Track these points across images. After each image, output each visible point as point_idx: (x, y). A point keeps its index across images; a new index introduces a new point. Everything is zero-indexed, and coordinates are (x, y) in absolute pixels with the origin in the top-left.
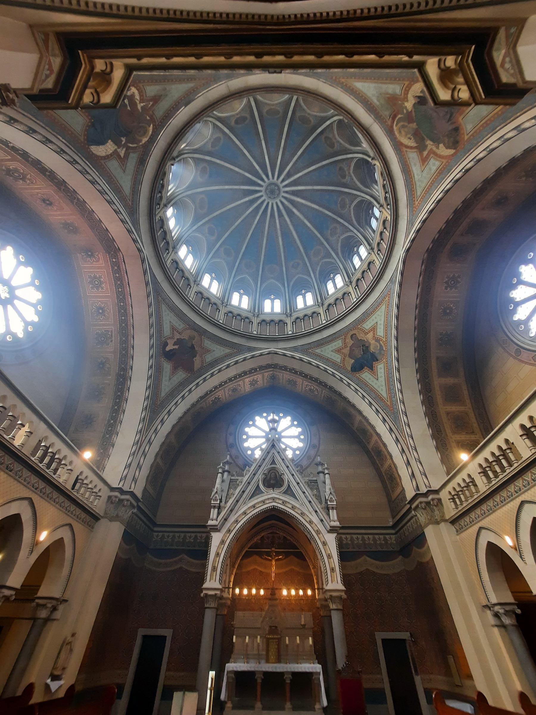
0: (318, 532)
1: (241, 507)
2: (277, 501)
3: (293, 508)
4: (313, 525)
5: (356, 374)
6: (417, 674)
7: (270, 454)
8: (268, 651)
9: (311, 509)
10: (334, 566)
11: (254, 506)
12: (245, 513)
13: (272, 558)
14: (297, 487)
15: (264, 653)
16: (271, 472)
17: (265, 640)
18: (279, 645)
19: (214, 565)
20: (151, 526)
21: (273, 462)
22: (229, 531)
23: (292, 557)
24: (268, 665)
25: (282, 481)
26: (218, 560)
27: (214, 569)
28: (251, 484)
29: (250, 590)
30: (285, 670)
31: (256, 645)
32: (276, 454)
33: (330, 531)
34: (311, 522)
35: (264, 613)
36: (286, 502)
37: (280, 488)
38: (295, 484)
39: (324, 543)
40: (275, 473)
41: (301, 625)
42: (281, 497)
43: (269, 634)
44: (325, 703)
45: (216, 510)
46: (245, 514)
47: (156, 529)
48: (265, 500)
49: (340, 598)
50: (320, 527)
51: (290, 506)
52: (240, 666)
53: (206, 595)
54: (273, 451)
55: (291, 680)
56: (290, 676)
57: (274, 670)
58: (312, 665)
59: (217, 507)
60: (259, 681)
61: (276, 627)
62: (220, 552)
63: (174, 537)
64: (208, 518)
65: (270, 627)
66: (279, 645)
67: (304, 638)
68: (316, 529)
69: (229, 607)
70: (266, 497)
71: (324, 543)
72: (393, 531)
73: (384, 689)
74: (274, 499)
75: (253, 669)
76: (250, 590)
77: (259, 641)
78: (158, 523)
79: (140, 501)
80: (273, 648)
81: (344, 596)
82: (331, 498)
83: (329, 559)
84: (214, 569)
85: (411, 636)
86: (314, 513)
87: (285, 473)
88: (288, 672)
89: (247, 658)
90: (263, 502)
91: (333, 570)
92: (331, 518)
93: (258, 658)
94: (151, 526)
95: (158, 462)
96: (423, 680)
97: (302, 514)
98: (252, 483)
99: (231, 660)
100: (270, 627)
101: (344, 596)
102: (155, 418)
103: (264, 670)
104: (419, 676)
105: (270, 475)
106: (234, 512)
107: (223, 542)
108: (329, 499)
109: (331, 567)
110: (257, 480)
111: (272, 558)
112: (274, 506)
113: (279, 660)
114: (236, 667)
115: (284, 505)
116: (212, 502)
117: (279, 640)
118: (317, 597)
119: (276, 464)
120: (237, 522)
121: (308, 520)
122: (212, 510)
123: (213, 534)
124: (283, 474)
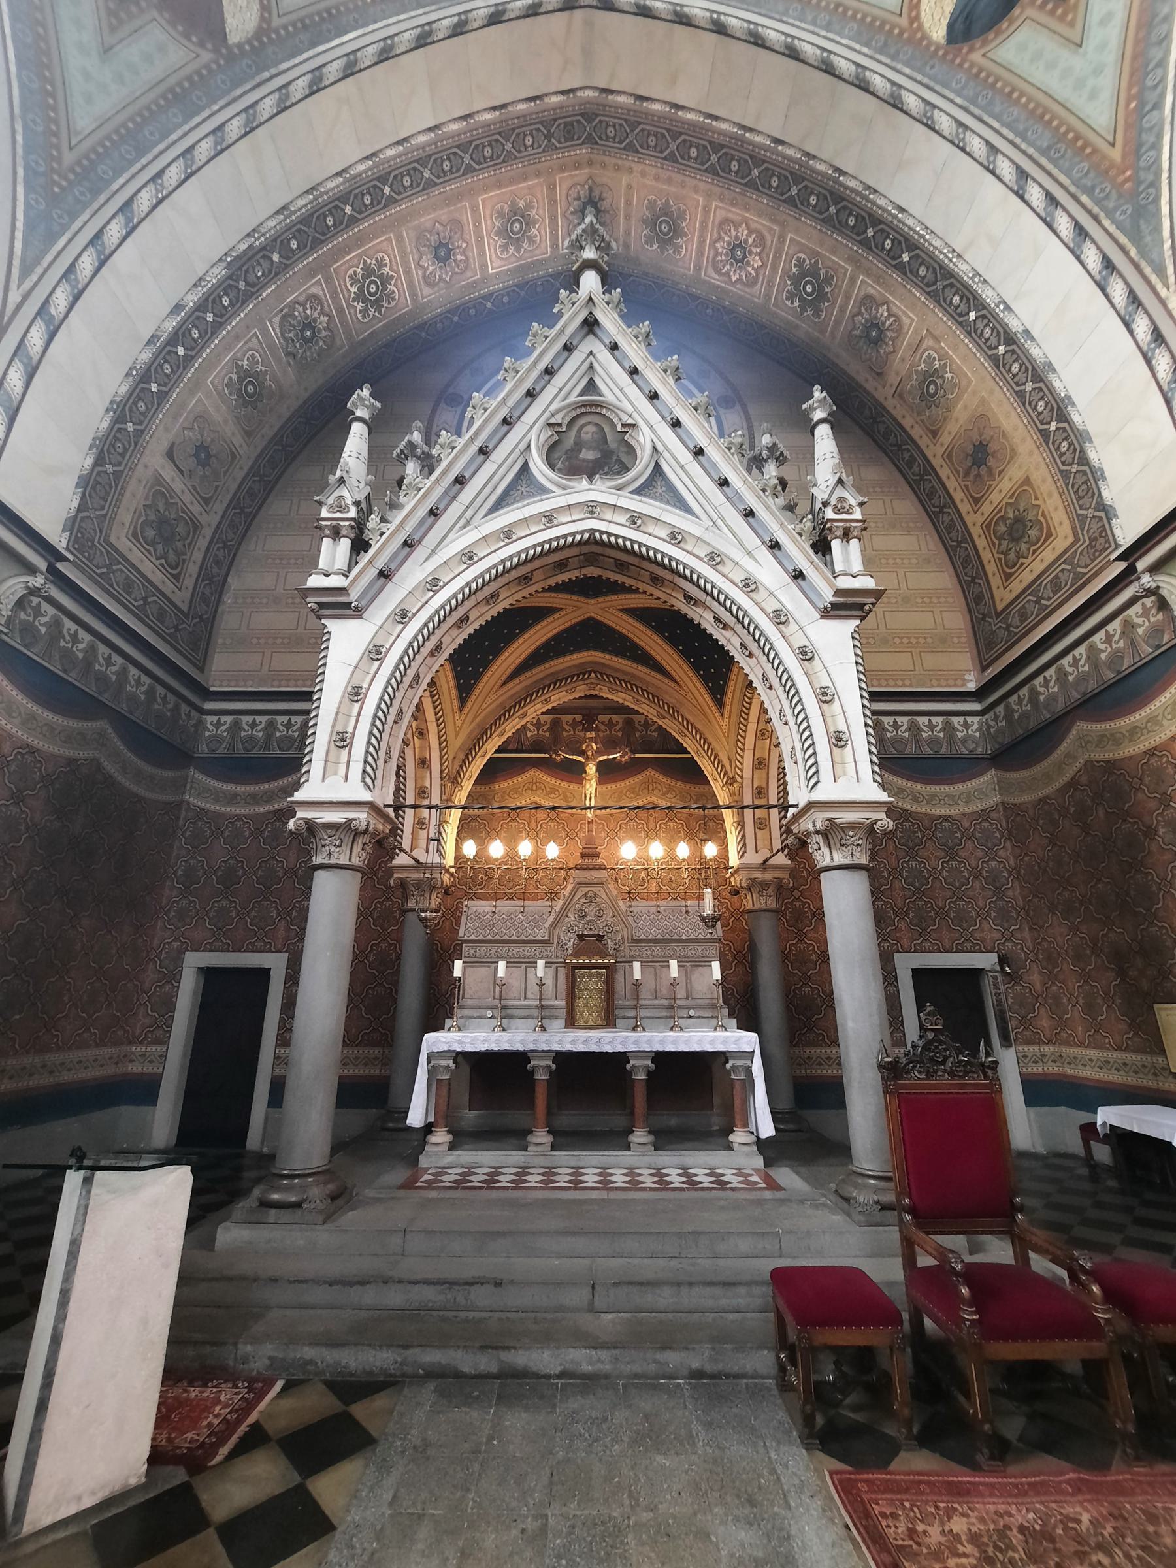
0: (780, 618)
1: (451, 536)
2: (608, 515)
3: (675, 537)
4: (761, 596)
5: (971, 50)
6: (1006, 1041)
7: (577, 357)
8: (571, 997)
9: (752, 541)
10: (842, 727)
11: (508, 534)
12: (468, 556)
13: (587, 758)
14: (694, 467)
15: (561, 1003)
16: (581, 422)
17: (562, 971)
18: (609, 984)
19: (339, 728)
20: (197, 701)
21: (591, 386)
22: (403, 616)
23: (650, 773)
24: (573, 1034)
25: (631, 451)
26: (355, 713)
27: (342, 740)
28: (493, 457)
29: (512, 854)
30: (632, 1048)
31: (532, 982)
32: (604, 355)
33: (833, 611)
34: (749, 586)
35: (559, 904)
36: (641, 516)
37: (618, 473)
38: (686, 457)
39: (804, 653)
40: (597, 425)
41: (703, 918)
42: (623, 502)
43: (576, 955)
44: (767, 1129)
45: (345, 544)
46: (471, 558)
47: (210, 706)
48: (559, 510)
49: (870, 830)
50: (791, 598)
51: (664, 533)
52: (474, 1040)
53: (311, 827)
54: (591, 344)
55: (649, 1073)
56: (649, 1062)
57: (594, 1048)
58: (720, 1034)
59: (344, 532)
60: (542, 1076)
61: (600, 938)
62: (365, 685)
63: (271, 725)
64: (311, 563)
65: (581, 937)
66: (609, 984)
67: (692, 964)
68: (771, 606)
69: (447, 891)
70: (561, 501)
71: (804, 653)
72: (976, 706)
73: (1029, 1103)
74: (592, 508)
75: (519, 1047)
76: (512, 854)
77: (540, 973)
78: (212, 689)
79: (64, 559)
80: (591, 990)
81: (884, 822)
82: (842, 499)
83: (825, 706)
84: (342, 740)
85: (1003, 960)
86: (764, 554)
87: (641, 423)
88: (641, 1054)
89: (505, 1014)
90: (549, 518)
91: (839, 739)
92: (838, 567)
93: (543, 1014)
94: (197, 701)
95: (158, 479)
96: (1021, 1059)
97: (714, 559)
98: (498, 456)
99: (448, 1023)
100: (581, 937)
101: (884, 822)
102: (64, 228)
103: (556, 1047)
104: (1012, 1050)
105: (579, 431)
106: (420, 552)
107: (376, 653)
108: (833, 501)
109: (832, 729)
110: (522, 446)
111: (587, 758)
112: (592, 531)
113: (609, 1020)
114: (459, 1042)
115: (638, 529)
116: (324, 513)
117: (611, 970)
118: (734, 861)
119: (601, 395)
120: (434, 584)
121: (738, 577)
122: (326, 542)
123: (332, 625)
124: (633, 426)
